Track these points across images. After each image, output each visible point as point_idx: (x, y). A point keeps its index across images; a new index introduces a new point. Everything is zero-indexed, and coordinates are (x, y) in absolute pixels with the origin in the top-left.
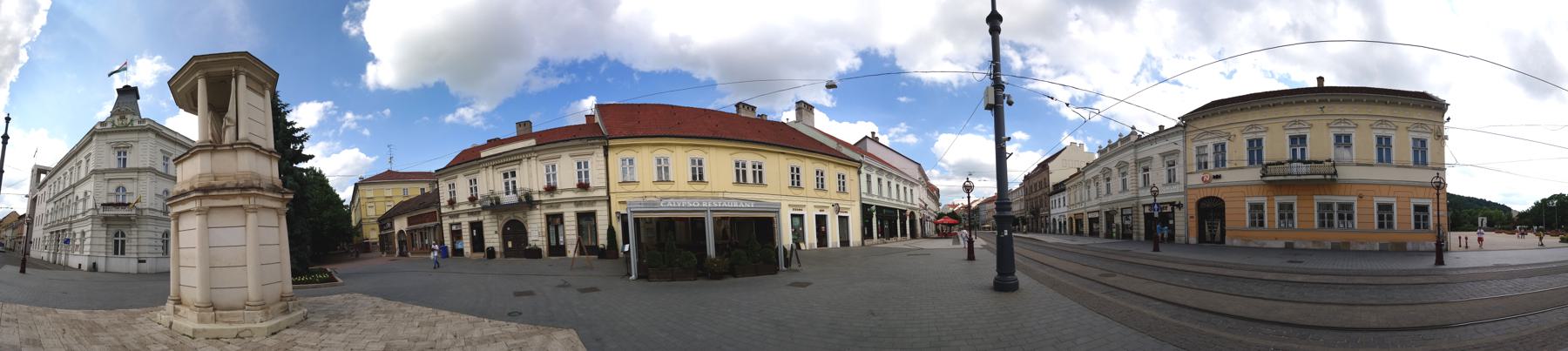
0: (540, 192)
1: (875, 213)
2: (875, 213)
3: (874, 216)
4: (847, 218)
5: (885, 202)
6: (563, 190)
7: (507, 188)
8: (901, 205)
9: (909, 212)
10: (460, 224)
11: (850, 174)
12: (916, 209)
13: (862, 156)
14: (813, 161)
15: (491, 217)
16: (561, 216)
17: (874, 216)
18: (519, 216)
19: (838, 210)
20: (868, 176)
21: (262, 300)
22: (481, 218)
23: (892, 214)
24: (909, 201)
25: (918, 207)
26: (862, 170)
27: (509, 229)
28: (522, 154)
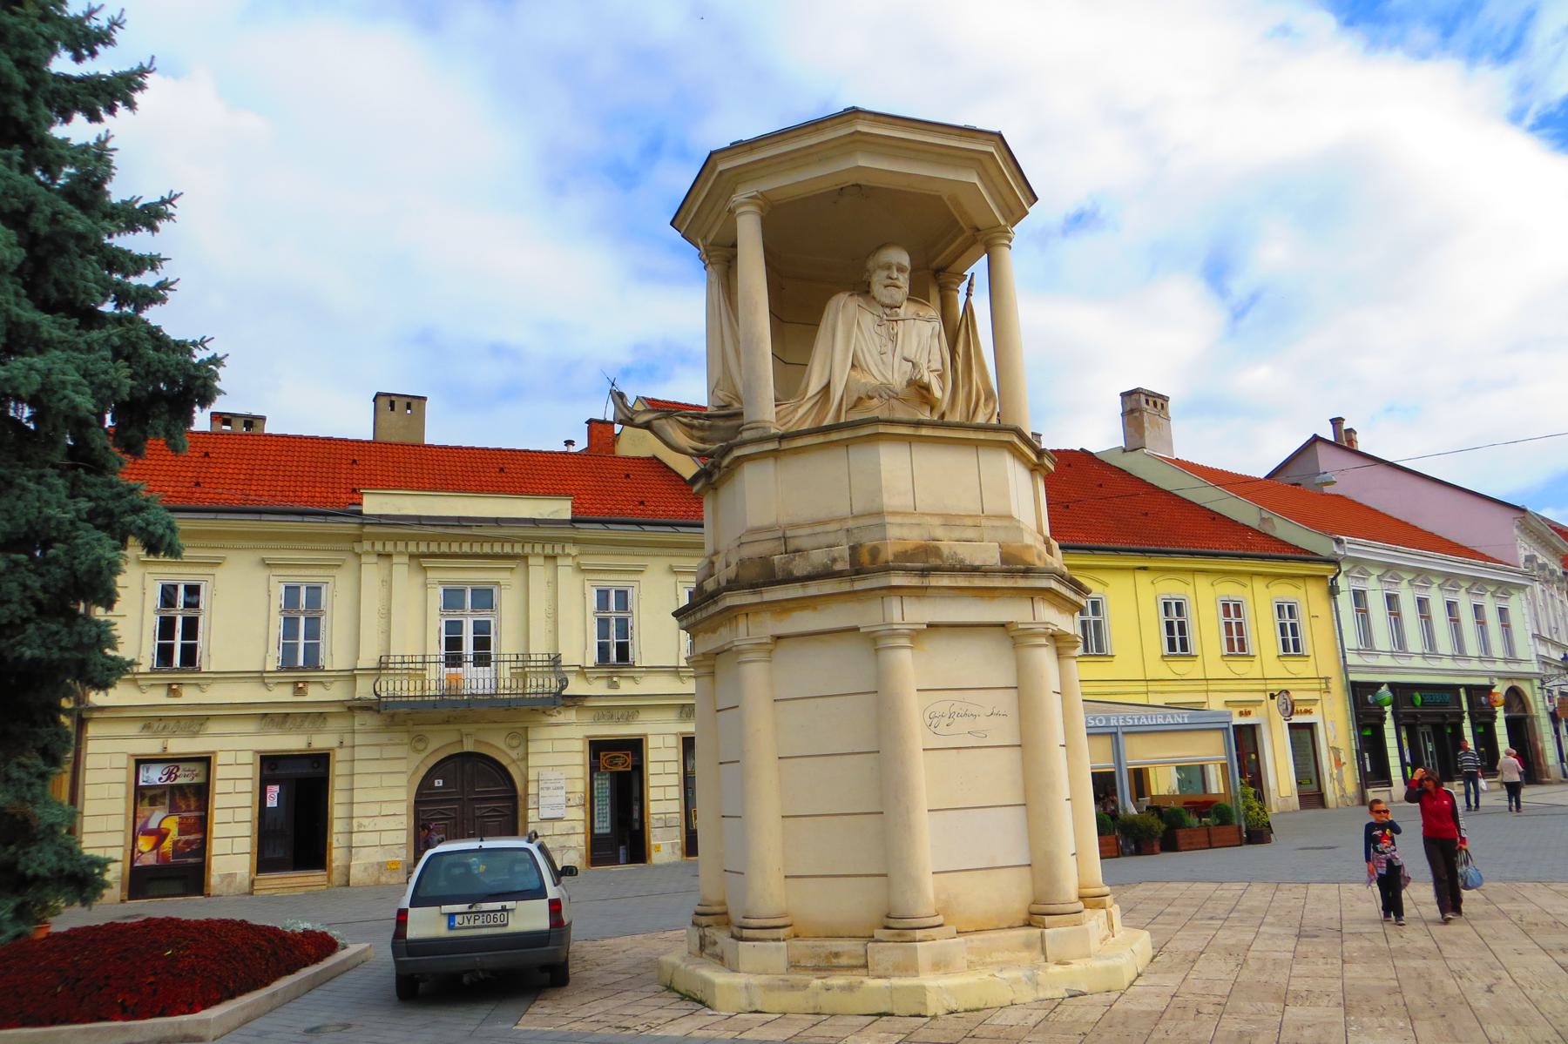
0: (582, 671)
1: (1388, 709)
2: (1388, 709)
3: (1388, 715)
4: (1310, 727)
5: (1417, 669)
6: (651, 670)
7: (453, 643)
8: (1471, 671)
9: (1500, 689)
10: (205, 761)
11: (1309, 599)
12: (1528, 677)
13: (1339, 542)
14: (1211, 579)
15: (383, 738)
16: (635, 746)
17: (1388, 715)
18: (497, 745)
19: (1290, 709)
20: (1359, 597)
21: (723, 903)
22: (321, 742)
23: (1443, 704)
24: (1498, 649)
25: (1535, 667)
26: (1342, 582)
27: (439, 783)
28: (534, 540)
